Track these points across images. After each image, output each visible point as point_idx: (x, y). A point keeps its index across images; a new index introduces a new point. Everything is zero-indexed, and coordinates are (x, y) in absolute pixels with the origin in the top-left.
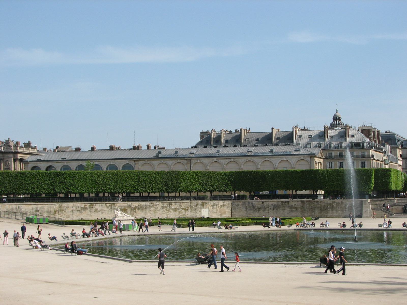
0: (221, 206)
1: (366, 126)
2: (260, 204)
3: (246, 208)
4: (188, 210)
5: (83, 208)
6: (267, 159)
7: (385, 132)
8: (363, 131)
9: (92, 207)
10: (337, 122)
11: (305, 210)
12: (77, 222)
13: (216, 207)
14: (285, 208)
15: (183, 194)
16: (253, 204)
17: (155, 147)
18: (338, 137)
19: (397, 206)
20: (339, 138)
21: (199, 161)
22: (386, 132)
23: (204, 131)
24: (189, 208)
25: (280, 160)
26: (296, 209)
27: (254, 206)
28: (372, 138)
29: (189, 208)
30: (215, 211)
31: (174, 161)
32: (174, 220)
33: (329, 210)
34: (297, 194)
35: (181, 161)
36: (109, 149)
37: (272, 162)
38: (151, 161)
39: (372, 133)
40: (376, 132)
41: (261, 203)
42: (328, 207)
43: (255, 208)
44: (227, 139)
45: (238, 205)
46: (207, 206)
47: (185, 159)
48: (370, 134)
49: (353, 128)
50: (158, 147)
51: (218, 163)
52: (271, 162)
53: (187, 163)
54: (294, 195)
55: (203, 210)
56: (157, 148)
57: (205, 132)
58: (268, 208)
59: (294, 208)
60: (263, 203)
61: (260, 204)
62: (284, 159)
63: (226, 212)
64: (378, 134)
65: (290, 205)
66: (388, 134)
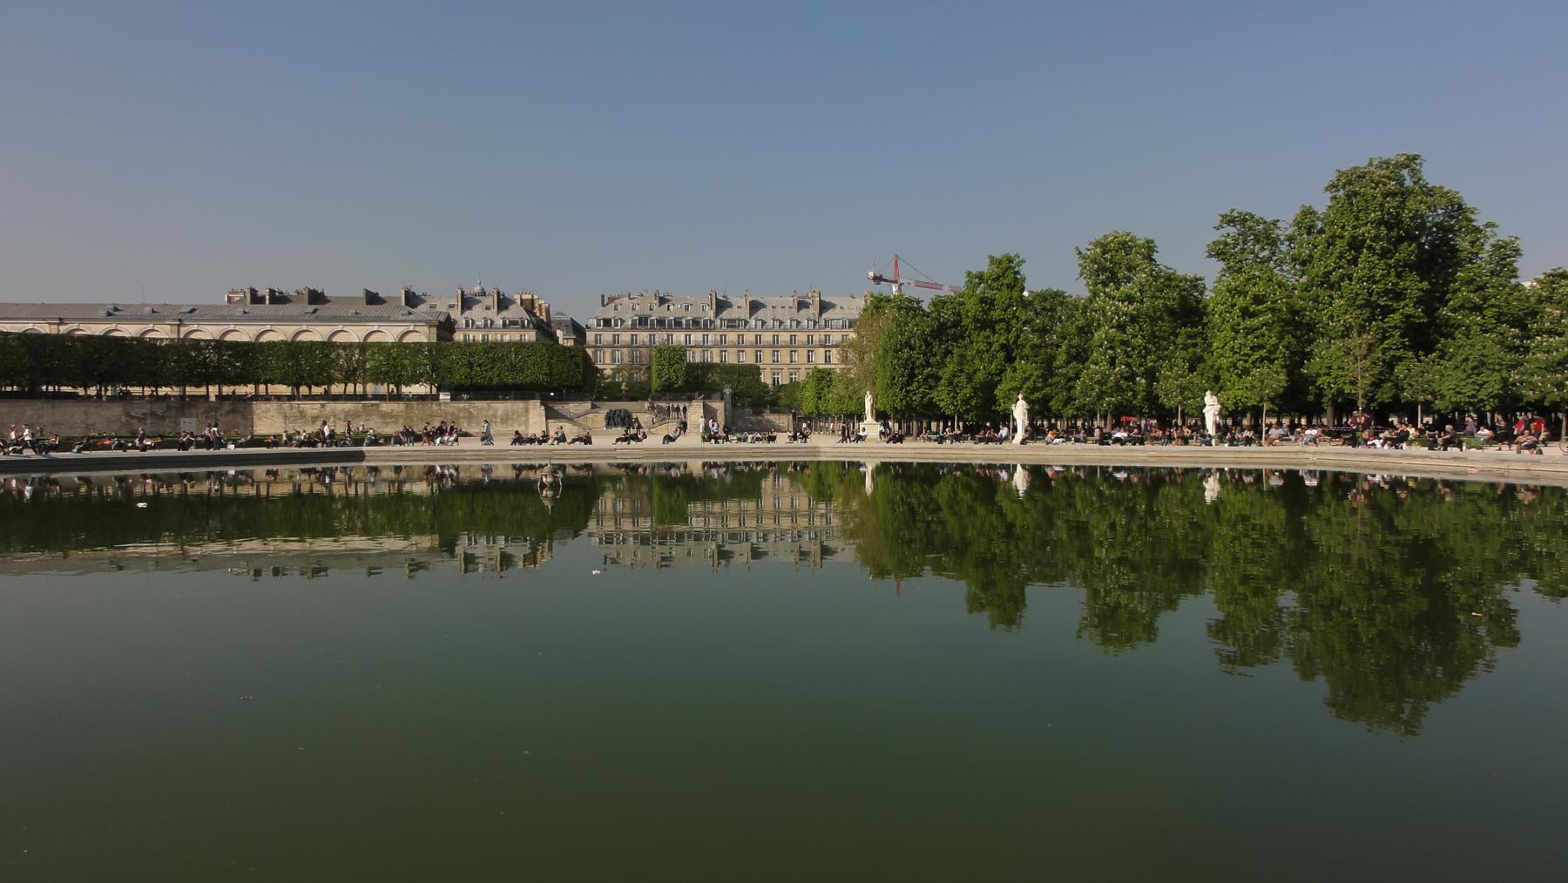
3: (285, 417)
4: (145, 419)
5: (782, 402)
9: (926, 487)
12: (572, 477)
13: (216, 415)
14: (372, 417)
24: (148, 416)
27: (302, 414)
32: (269, 436)
36: (767, 484)
42: (461, 414)
43: (305, 417)
45: (267, 411)
46: (194, 411)
54: (214, 384)
55: (183, 420)
58: (334, 416)
59: (391, 419)
60: (323, 406)
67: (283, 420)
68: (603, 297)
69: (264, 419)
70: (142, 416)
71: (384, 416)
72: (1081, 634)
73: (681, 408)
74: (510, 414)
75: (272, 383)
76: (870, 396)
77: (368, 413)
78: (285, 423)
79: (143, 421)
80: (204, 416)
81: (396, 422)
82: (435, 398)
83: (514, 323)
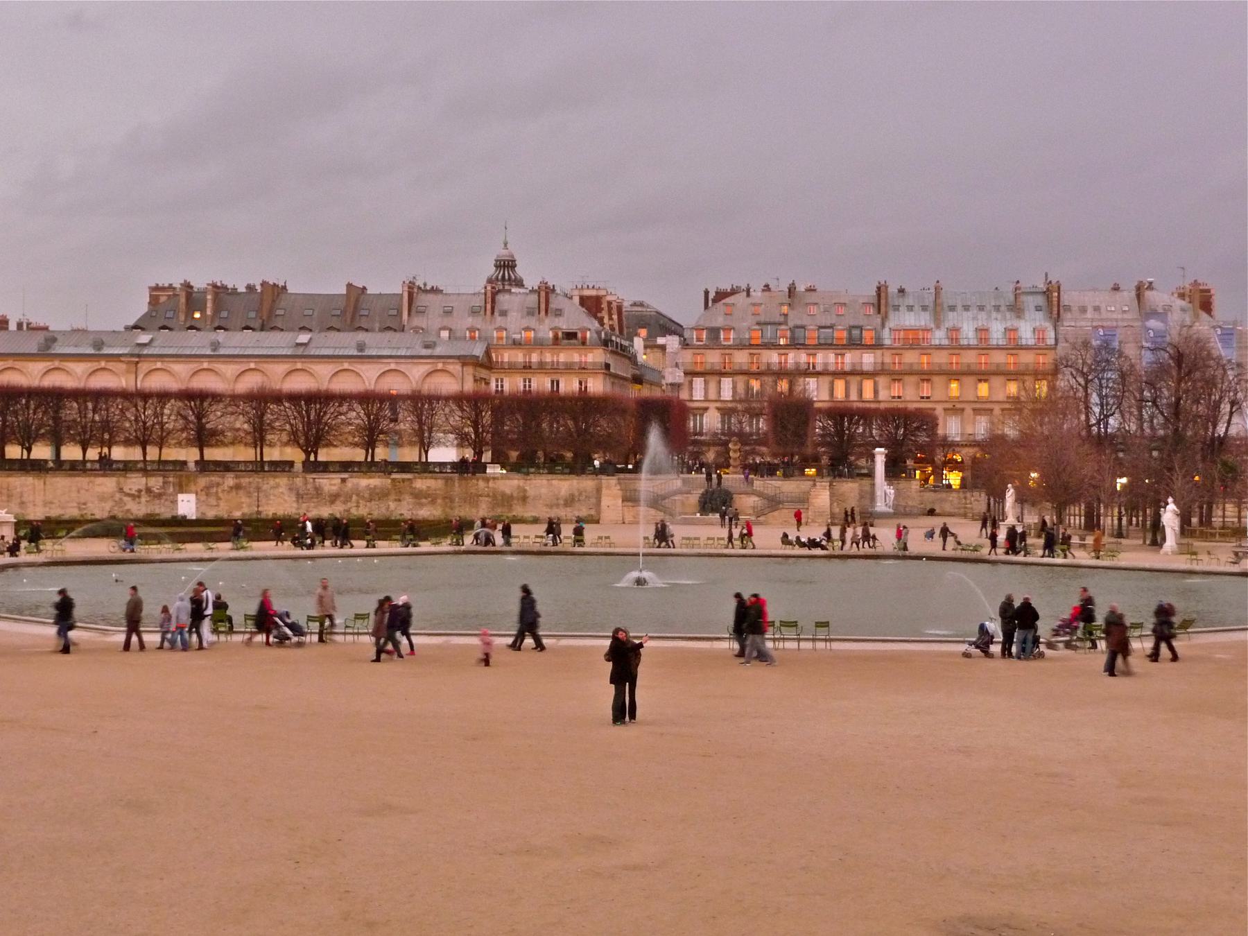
0: (231, 488)
1: (591, 287)
2: (335, 485)
4: (139, 497)
6: (346, 366)
7: (631, 305)
8: (584, 301)
10: (506, 273)
11: (452, 501)
13: (217, 492)
15: (118, 453)
16: (317, 484)
17: (20, 326)
18: (520, 315)
19: (685, 495)
20: (522, 317)
21: (159, 365)
22: (635, 304)
23: (160, 285)
25: (382, 371)
26: (430, 499)
27: (318, 490)
28: (606, 320)
29: (143, 493)
30: (213, 501)
31: (89, 364)
33: (516, 502)
34: (206, 458)
35: (111, 365)
37: (361, 374)
38: (25, 364)
39: (604, 305)
40: (614, 305)
41: (340, 480)
43: (321, 494)
44: (897, 312)
45: (278, 486)
47: (122, 359)
48: (601, 310)
49: (558, 291)
50: (28, 324)
51: (214, 373)
52: (357, 373)
53: (128, 372)
56: (25, 327)
57: (163, 289)
58: (358, 495)
59: (426, 498)
60: (343, 480)
61: (335, 485)
62: (393, 366)
63: (244, 505)
64: (620, 308)
65: (415, 488)
66: (640, 309)
67: (294, 499)
68: (707, 293)
69: (272, 497)
70: (136, 493)
71: (418, 495)
72: (294, 492)
73: (737, 543)
74: (577, 494)
75: (794, 650)
76: (1012, 491)
77: (398, 491)
78: (298, 501)
79: (137, 499)
80: (203, 493)
81: (433, 502)
82: (478, 467)
83: (571, 336)
